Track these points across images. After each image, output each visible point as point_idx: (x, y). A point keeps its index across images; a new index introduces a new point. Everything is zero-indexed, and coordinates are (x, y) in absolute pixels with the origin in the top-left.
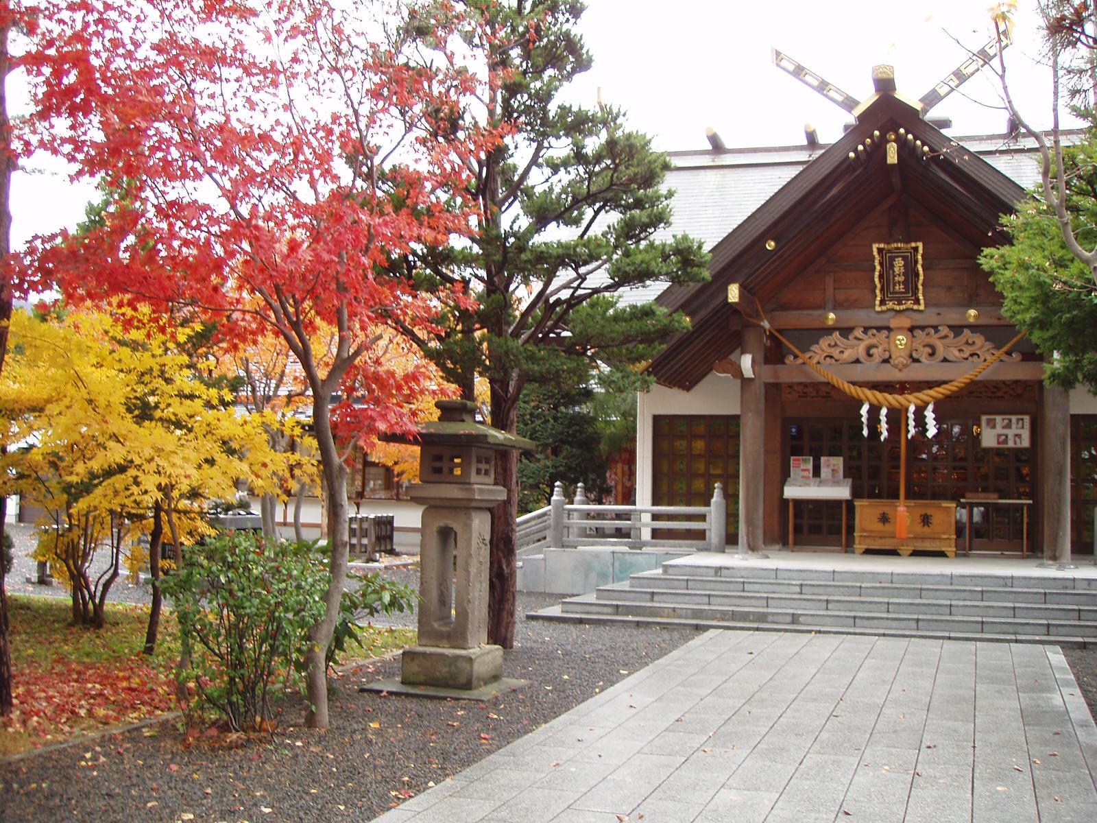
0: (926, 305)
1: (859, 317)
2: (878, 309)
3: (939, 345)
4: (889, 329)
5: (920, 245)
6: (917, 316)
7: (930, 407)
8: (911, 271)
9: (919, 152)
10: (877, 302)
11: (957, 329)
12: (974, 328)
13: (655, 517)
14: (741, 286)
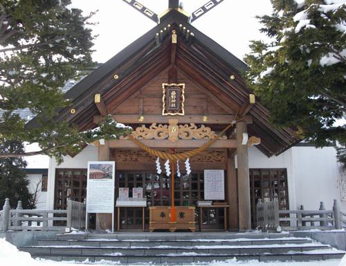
0: (185, 114)
1: (153, 120)
2: (163, 114)
3: (190, 131)
4: (168, 125)
5: (184, 85)
6: (181, 118)
7: (188, 160)
8: (179, 98)
9: (184, 32)
10: (163, 111)
11: (198, 126)
12: (206, 125)
13: (55, 215)
14: (101, 96)
